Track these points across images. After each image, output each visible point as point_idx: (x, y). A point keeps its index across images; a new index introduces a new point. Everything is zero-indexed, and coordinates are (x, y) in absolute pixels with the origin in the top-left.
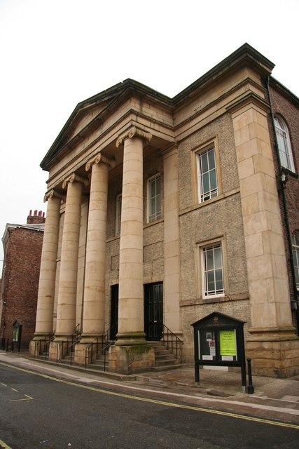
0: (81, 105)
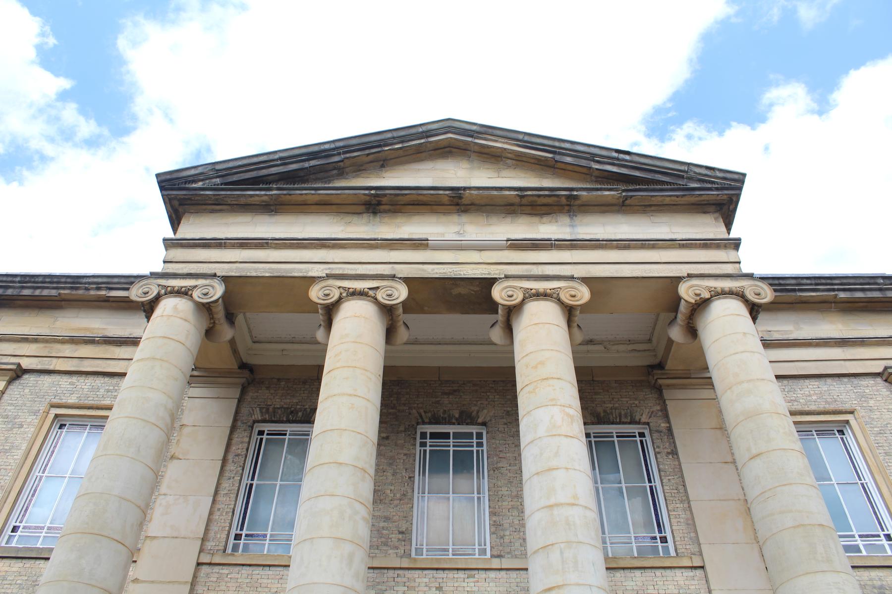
0: (449, 126)
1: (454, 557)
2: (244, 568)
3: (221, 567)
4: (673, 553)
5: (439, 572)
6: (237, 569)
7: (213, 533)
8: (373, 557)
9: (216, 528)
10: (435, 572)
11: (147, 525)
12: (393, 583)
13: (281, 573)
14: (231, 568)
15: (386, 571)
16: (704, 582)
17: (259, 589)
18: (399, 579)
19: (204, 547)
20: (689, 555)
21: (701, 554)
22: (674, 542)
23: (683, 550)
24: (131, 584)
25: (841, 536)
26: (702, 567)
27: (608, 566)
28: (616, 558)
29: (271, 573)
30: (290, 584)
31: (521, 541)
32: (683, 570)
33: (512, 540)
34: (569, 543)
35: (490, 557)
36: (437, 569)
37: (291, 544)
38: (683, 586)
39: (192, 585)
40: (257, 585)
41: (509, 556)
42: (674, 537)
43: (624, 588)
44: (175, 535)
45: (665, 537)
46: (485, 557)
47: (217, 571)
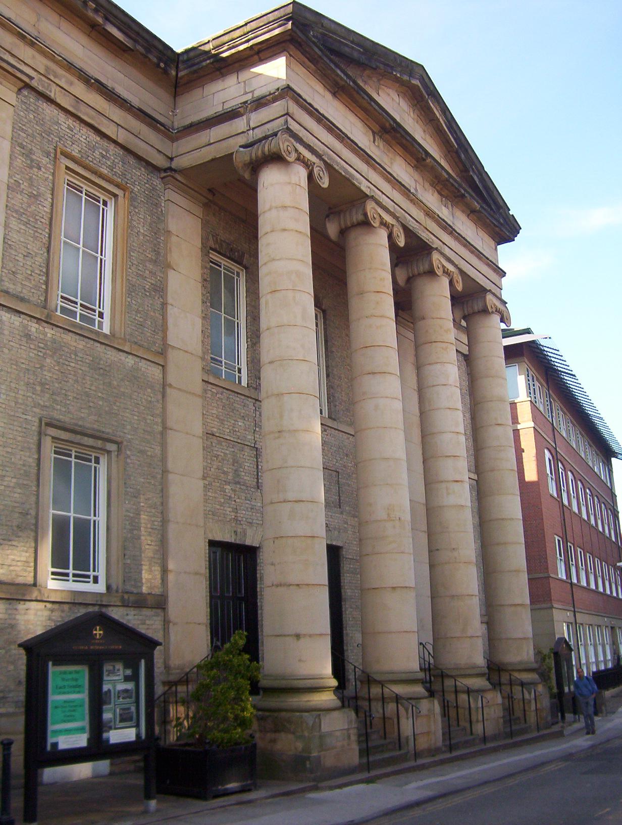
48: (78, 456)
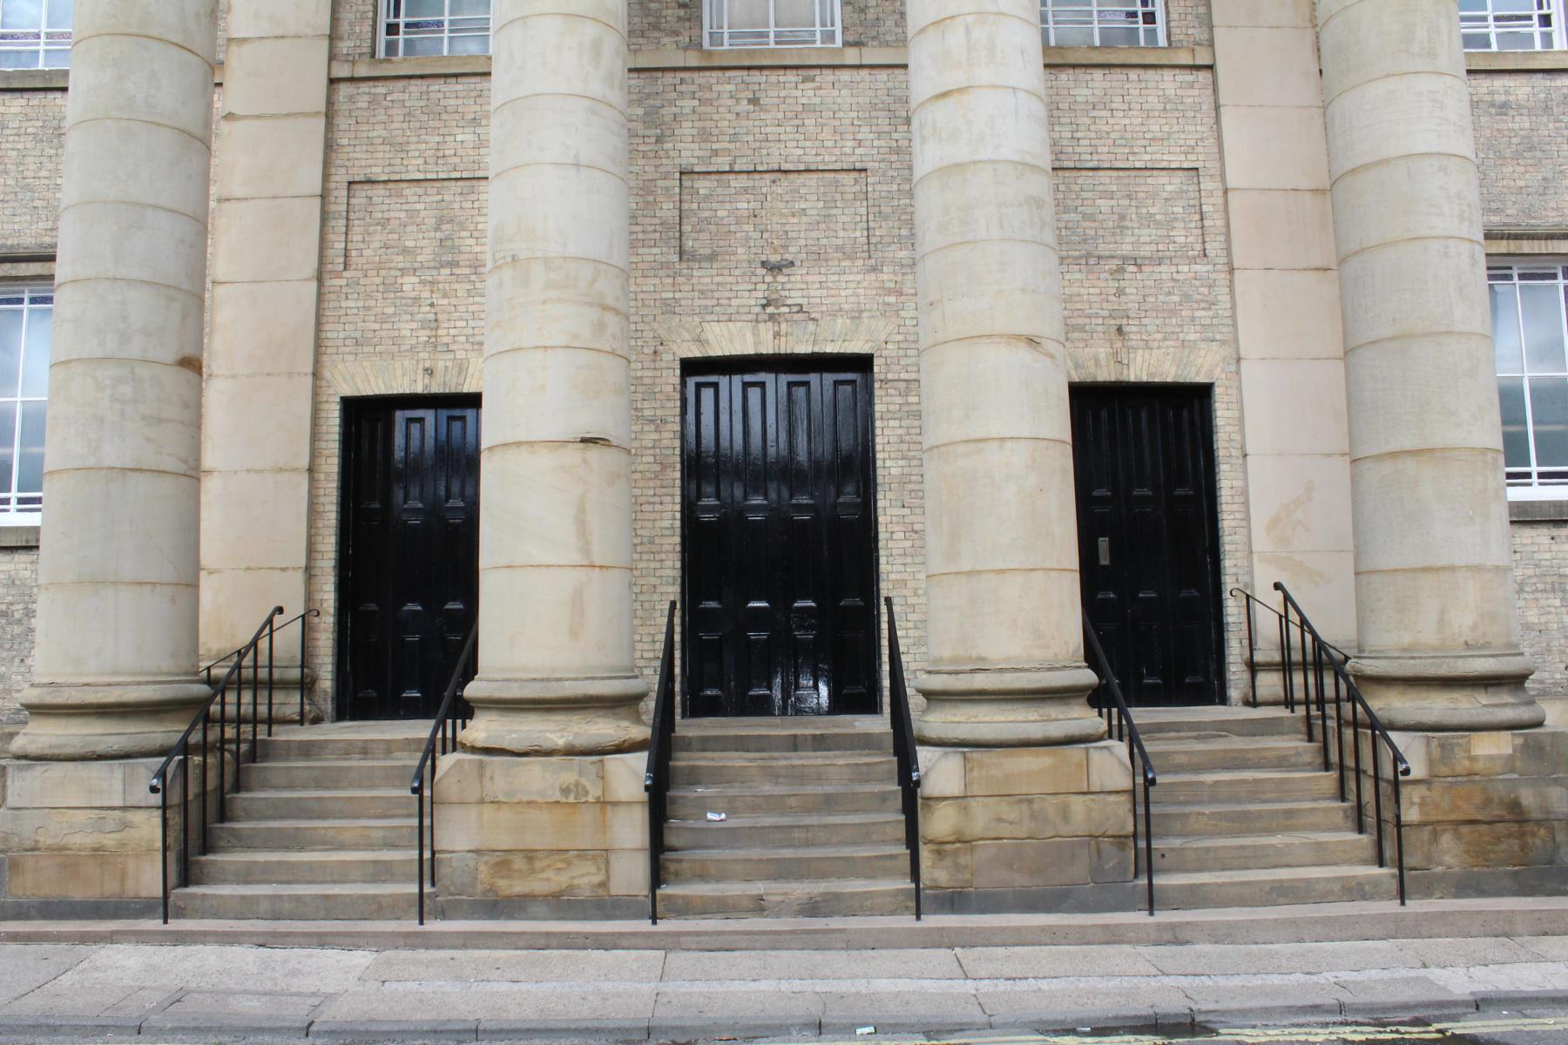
1: (779, 47)
2: (413, 82)
3: (371, 83)
4: (1162, 41)
5: (752, 72)
6: (401, 84)
7: (346, 24)
8: (635, 51)
9: (349, 15)
10: (745, 73)
11: (225, 18)
12: (674, 95)
13: (479, 87)
14: (391, 85)
15: (660, 74)
16: (1210, 92)
17: (444, 116)
18: (683, 88)
19: (337, 51)
20: (1191, 45)
21: (1211, 44)
22: (1168, 22)
23: (1182, 37)
24: (222, 122)
25: (1463, 19)
26: (1210, 67)
27: (1047, 62)
28: (1062, 48)
29: (459, 87)
30: (497, 99)
31: (897, 17)
32: (1177, 71)
33: (880, 15)
34: (981, 14)
35: (841, 46)
36: (749, 68)
37: (488, 36)
38: (1173, 97)
39: (327, 116)
40: (438, 109)
41: (875, 43)
42: (1168, 13)
43: (1071, 99)
44: (280, 32)
45: (1153, 14)
46: (834, 46)
47: (367, 90)
48: (1492, 275)
